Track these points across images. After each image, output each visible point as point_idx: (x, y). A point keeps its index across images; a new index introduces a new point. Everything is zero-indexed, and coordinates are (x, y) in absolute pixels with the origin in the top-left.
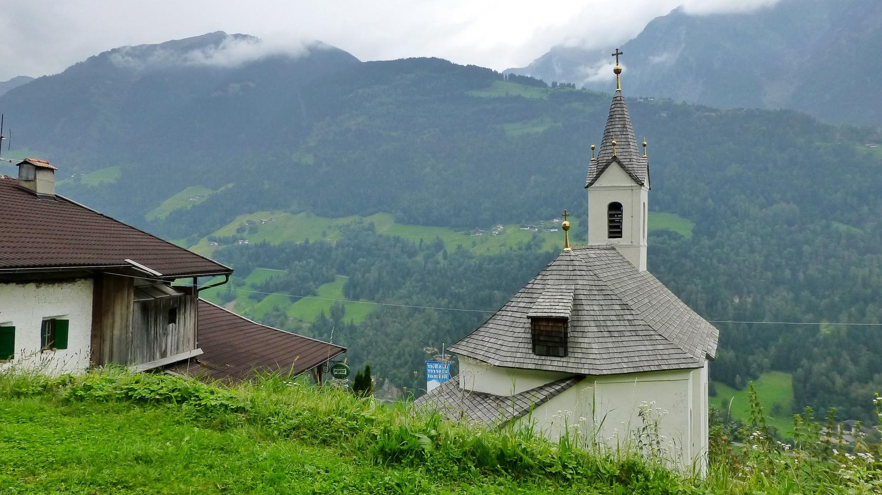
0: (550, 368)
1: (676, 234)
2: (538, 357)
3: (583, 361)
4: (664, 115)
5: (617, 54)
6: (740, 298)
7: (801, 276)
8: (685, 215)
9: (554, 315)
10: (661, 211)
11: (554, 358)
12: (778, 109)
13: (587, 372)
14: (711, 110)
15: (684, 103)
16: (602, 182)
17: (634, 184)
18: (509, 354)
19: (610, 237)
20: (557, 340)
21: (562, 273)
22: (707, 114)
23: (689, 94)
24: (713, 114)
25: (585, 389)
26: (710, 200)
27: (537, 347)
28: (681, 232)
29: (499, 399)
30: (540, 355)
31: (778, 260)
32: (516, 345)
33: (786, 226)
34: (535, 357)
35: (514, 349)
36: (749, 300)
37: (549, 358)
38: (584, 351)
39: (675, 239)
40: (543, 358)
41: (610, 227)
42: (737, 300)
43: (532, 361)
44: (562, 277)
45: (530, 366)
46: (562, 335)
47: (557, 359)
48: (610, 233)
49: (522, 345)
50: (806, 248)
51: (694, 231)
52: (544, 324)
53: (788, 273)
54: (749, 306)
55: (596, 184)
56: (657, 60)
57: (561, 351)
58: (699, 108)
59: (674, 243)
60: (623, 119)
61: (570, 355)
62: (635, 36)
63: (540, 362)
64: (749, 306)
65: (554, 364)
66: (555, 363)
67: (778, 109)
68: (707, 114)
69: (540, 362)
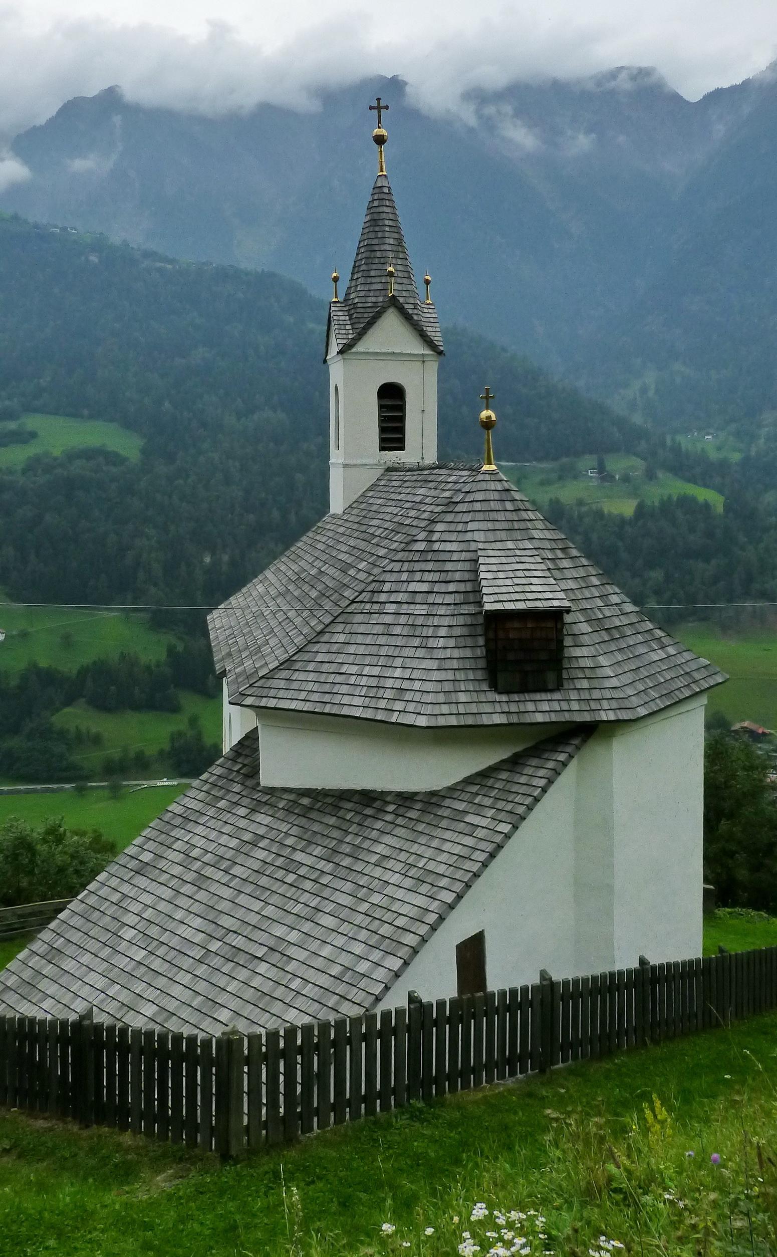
0: (539, 718)
1: (117, 455)
2: (504, 698)
3: (596, 694)
4: (94, 258)
5: (379, 108)
6: (213, 554)
7: (293, 518)
8: (129, 424)
9: (538, 604)
10: (91, 417)
11: (538, 696)
12: (260, 270)
13: (612, 716)
14: (172, 261)
15: (125, 244)
16: (371, 343)
17: (428, 352)
18: (441, 698)
19: (382, 449)
20: (543, 656)
21: (494, 515)
22: (158, 264)
23: (129, 231)
24: (169, 266)
25: (595, 752)
26: (167, 404)
27: (501, 678)
28: (123, 453)
29: (430, 802)
30: (508, 692)
31: (263, 495)
32: (450, 675)
33: (272, 445)
34: (498, 697)
35: (448, 687)
36: (226, 558)
37: (527, 696)
38: (588, 673)
39: (114, 464)
40: (516, 697)
41: (382, 430)
42: (208, 560)
43: (495, 710)
44: (498, 525)
45: (358, 713)
46: (553, 646)
47: (543, 696)
48: (382, 440)
49: (460, 675)
50: (299, 477)
51: (143, 451)
52: (516, 625)
53: (276, 514)
54: (225, 568)
55: (360, 347)
56: (79, 165)
57: (551, 677)
58: (147, 254)
59: (114, 470)
60: (396, 229)
61: (565, 684)
62: (42, 120)
63: (513, 708)
64: (225, 568)
65: (542, 709)
66: (545, 707)
67: (260, 270)
68: (158, 264)
69: (513, 708)
